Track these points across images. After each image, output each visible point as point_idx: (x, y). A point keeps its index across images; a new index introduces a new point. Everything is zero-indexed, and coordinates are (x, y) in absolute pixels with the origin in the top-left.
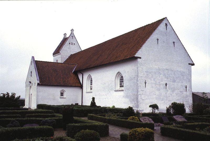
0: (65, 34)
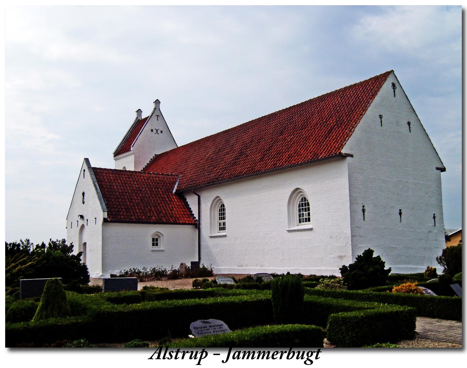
0: (139, 111)
